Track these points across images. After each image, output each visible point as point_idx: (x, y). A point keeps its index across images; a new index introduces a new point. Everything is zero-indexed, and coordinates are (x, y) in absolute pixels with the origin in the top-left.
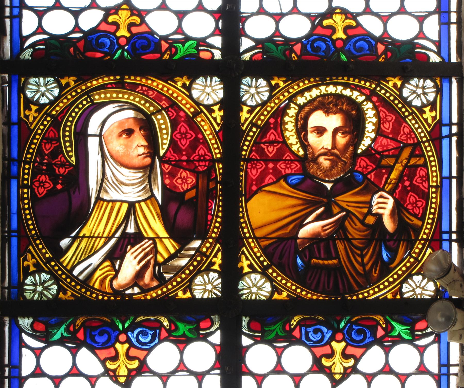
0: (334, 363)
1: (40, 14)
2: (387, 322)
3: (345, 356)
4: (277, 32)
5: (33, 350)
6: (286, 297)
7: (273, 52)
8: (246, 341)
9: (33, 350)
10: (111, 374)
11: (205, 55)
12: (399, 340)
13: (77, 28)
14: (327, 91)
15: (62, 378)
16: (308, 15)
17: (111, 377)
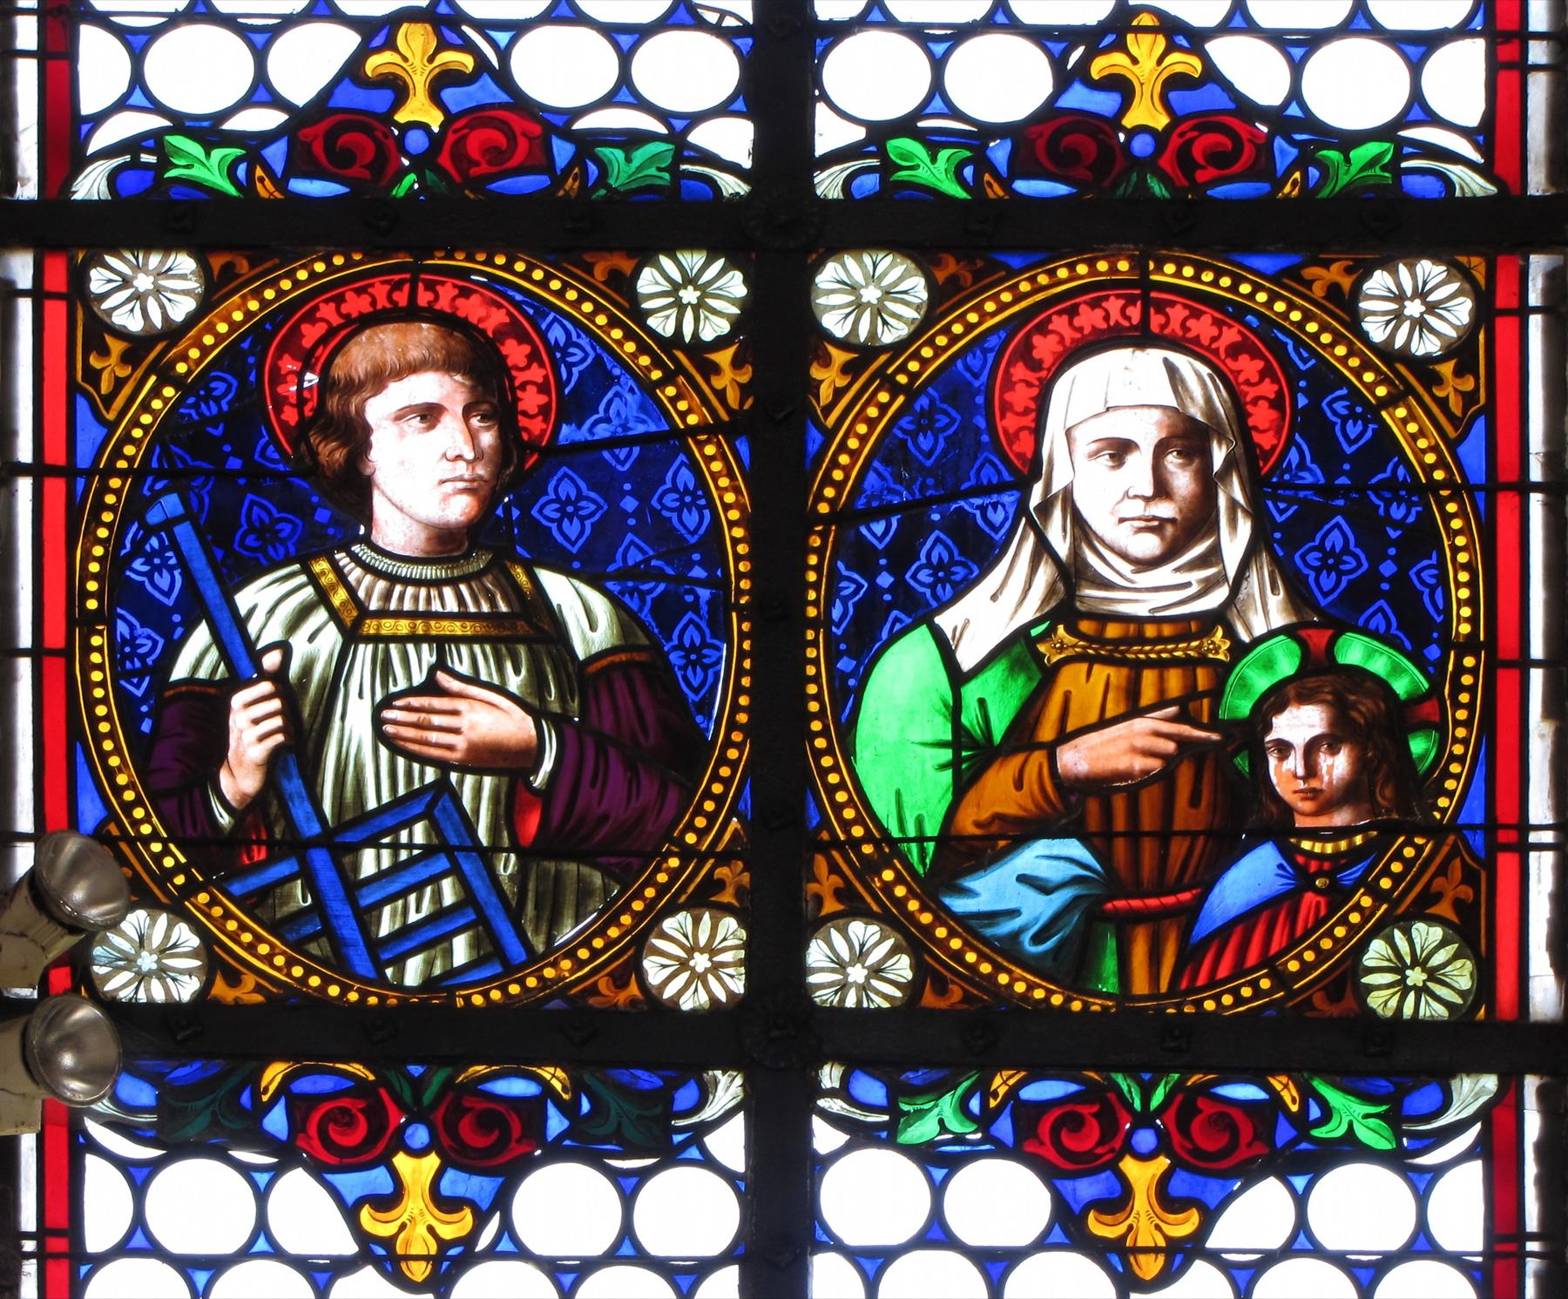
0: (431, 59)
1: (137, 42)
2: (1307, 1093)
3: (1168, 1201)
4: (628, 1188)
5: (123, 1164)
6: (961, 1002)
7: (639, 1117)
8: (825, 1138)
9: (123, 1164)
10: (380, 1251)
11: (872, 1090)
12: (1350, 1149)
13: (262, 92)
14: (1080, 329)
15: (217, 1265)
16: (1040, 35)
17: (379, 1263)
